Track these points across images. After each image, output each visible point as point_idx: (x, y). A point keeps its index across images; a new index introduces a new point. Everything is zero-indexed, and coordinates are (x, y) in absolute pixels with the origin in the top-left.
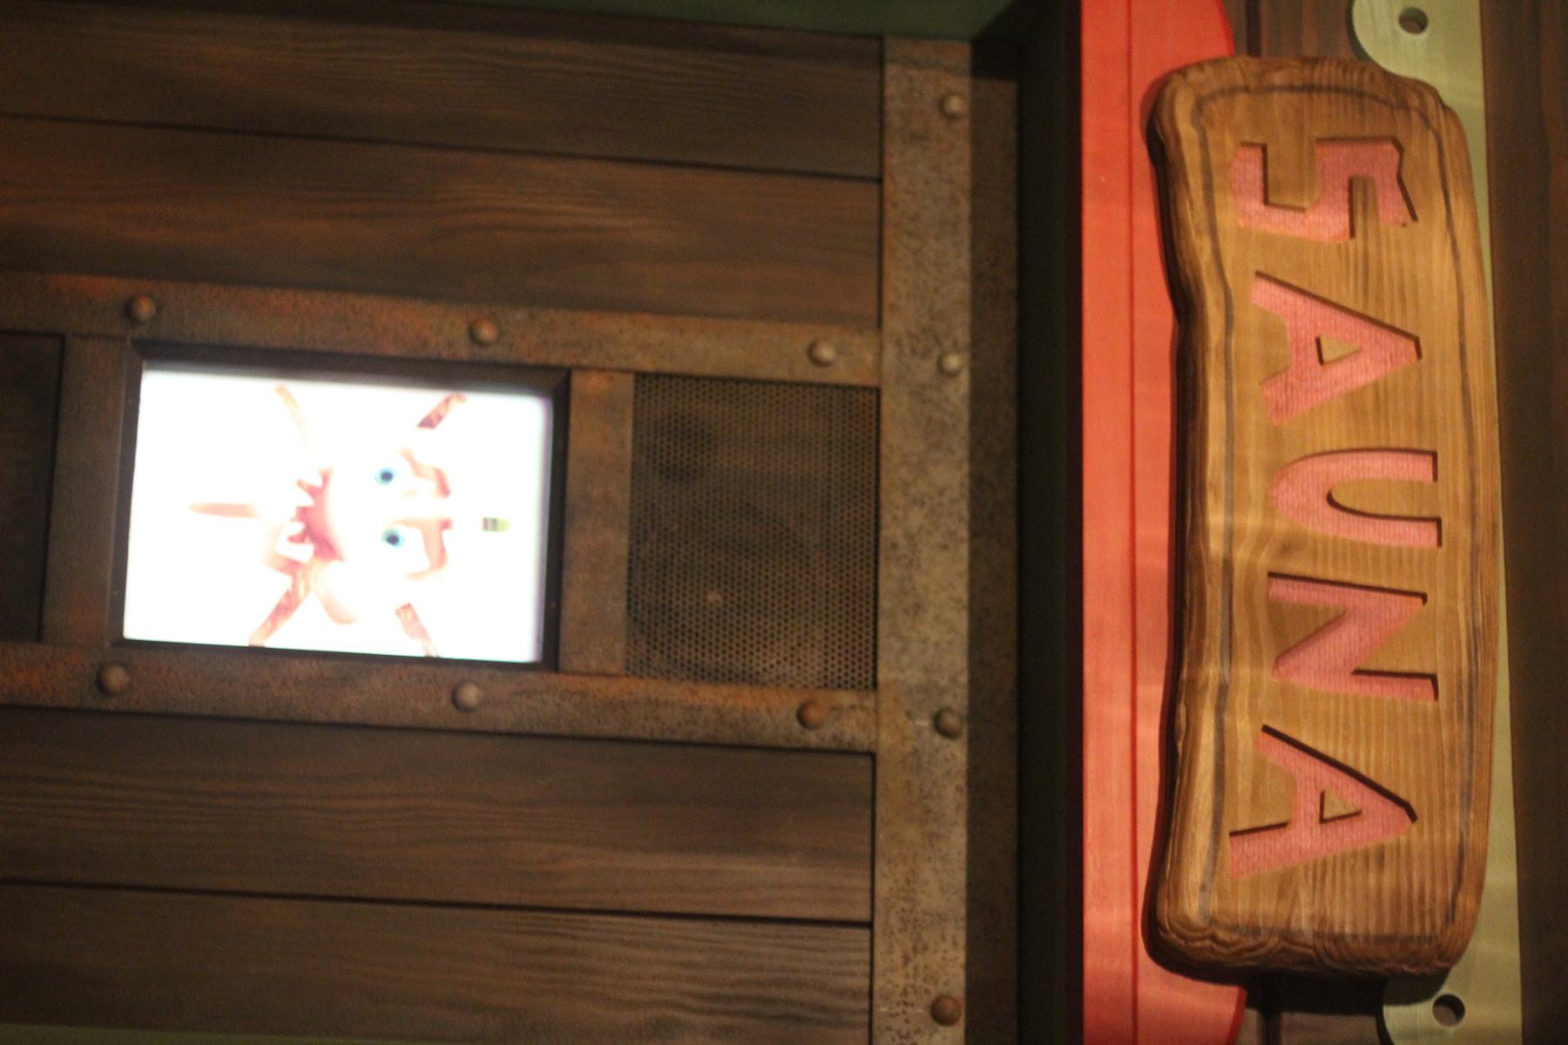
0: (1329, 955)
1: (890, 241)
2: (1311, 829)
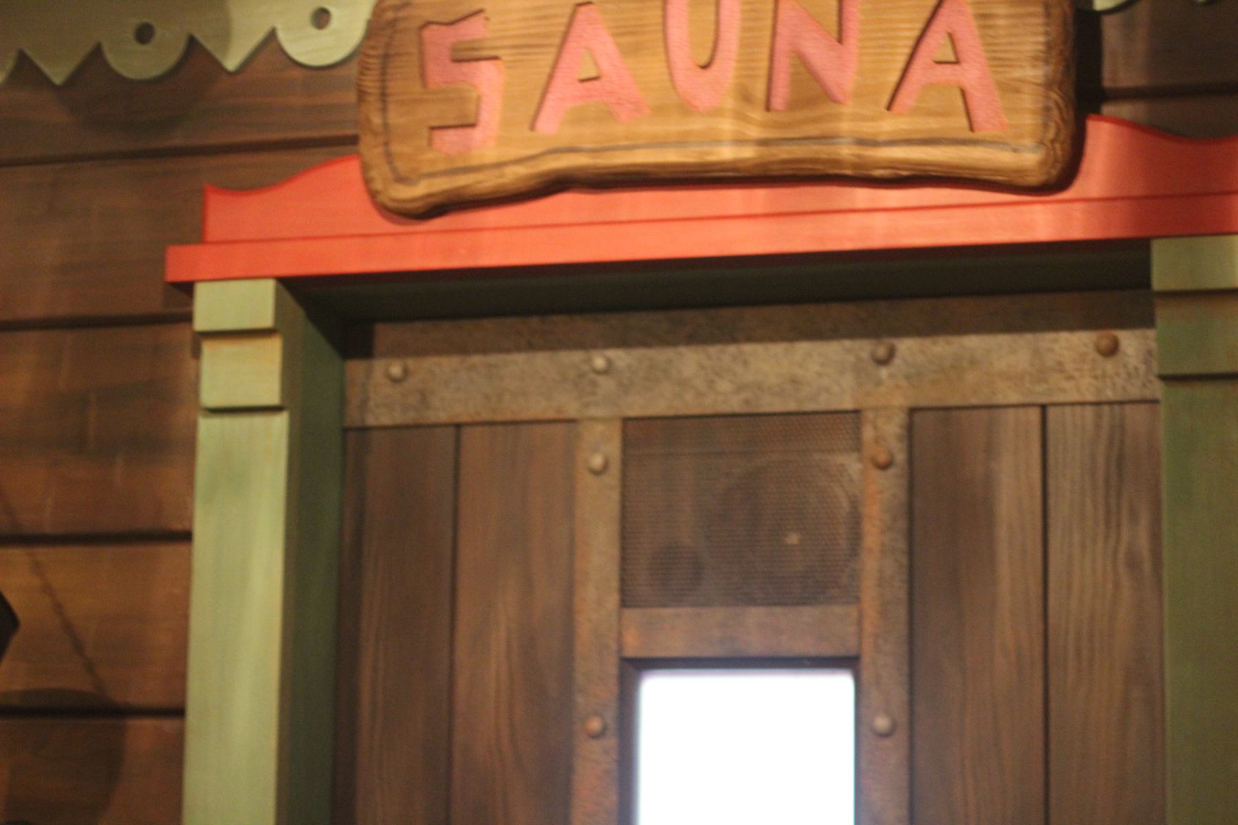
1: (507, 416)
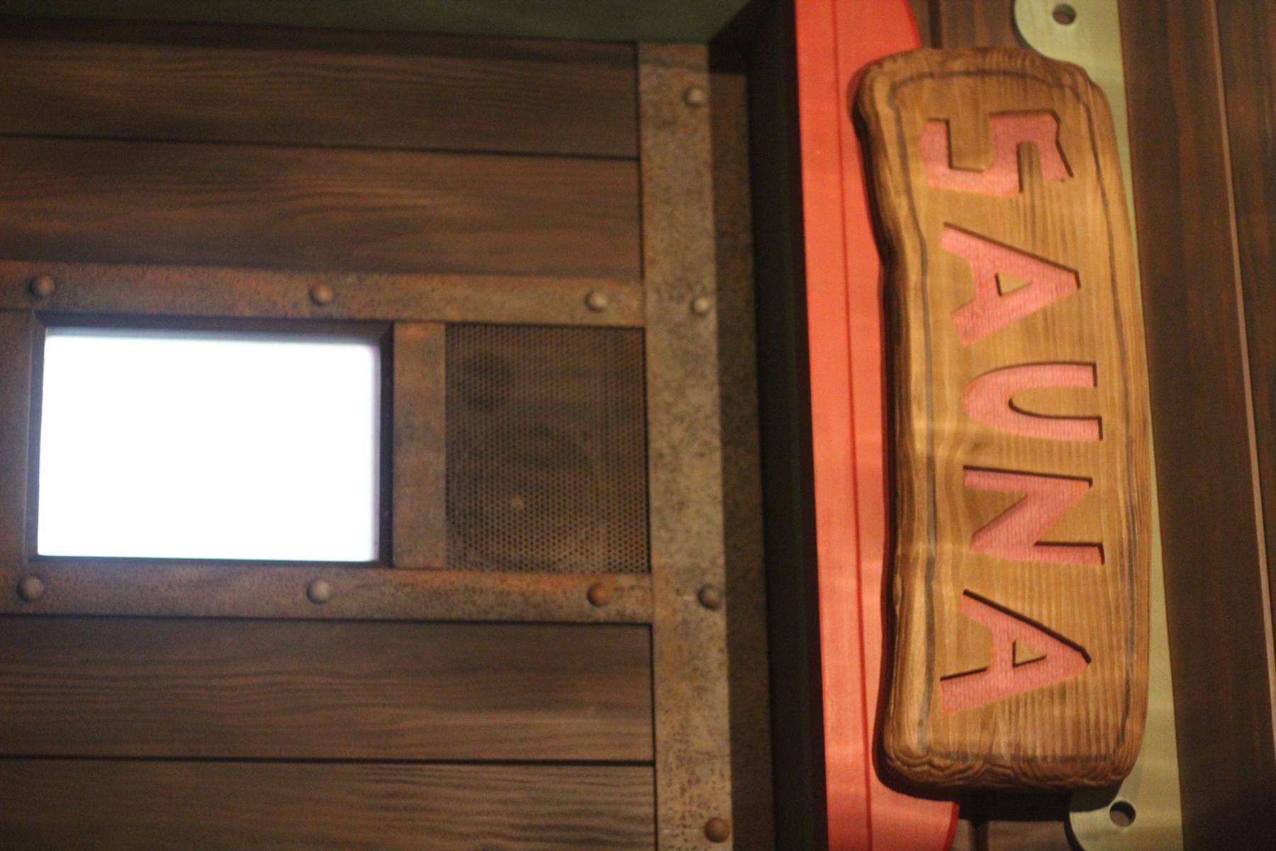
0: (1025, 774)
1: (648, 209)
2: (1006, 673)
